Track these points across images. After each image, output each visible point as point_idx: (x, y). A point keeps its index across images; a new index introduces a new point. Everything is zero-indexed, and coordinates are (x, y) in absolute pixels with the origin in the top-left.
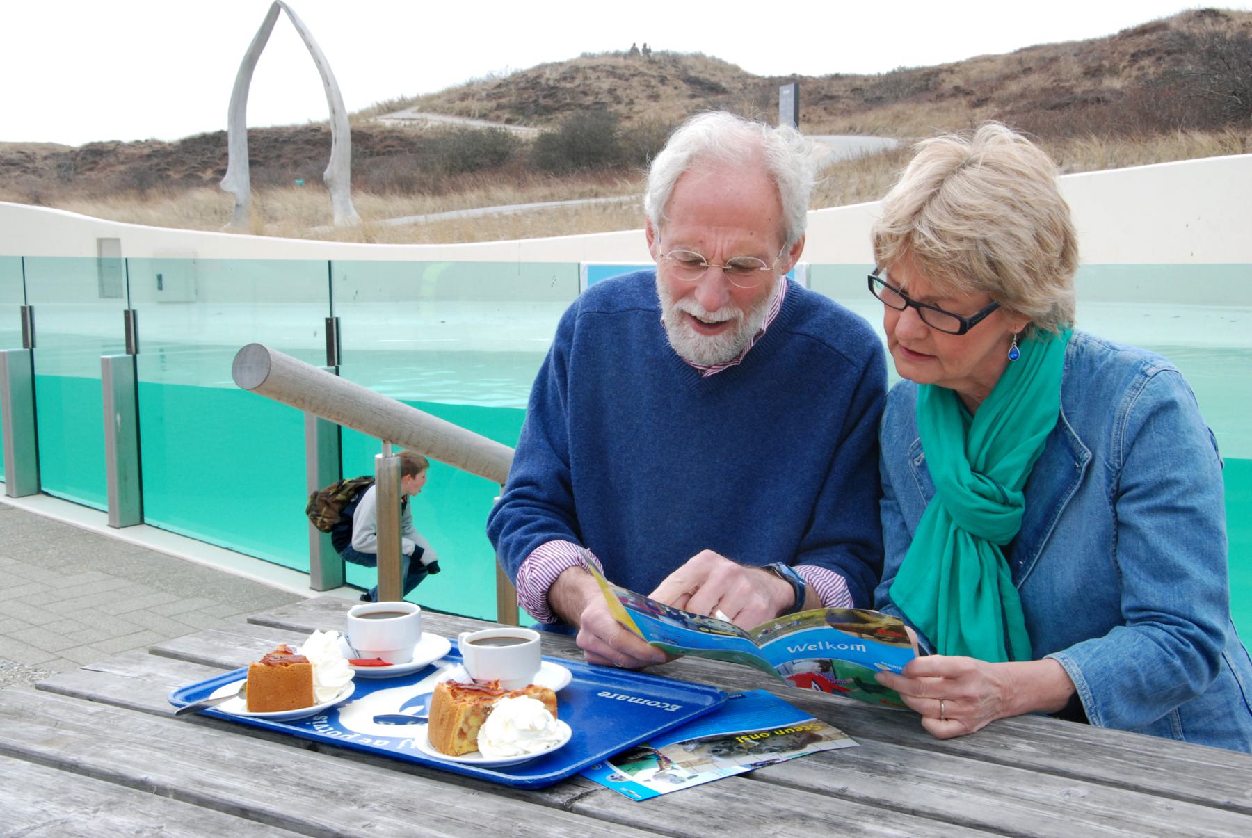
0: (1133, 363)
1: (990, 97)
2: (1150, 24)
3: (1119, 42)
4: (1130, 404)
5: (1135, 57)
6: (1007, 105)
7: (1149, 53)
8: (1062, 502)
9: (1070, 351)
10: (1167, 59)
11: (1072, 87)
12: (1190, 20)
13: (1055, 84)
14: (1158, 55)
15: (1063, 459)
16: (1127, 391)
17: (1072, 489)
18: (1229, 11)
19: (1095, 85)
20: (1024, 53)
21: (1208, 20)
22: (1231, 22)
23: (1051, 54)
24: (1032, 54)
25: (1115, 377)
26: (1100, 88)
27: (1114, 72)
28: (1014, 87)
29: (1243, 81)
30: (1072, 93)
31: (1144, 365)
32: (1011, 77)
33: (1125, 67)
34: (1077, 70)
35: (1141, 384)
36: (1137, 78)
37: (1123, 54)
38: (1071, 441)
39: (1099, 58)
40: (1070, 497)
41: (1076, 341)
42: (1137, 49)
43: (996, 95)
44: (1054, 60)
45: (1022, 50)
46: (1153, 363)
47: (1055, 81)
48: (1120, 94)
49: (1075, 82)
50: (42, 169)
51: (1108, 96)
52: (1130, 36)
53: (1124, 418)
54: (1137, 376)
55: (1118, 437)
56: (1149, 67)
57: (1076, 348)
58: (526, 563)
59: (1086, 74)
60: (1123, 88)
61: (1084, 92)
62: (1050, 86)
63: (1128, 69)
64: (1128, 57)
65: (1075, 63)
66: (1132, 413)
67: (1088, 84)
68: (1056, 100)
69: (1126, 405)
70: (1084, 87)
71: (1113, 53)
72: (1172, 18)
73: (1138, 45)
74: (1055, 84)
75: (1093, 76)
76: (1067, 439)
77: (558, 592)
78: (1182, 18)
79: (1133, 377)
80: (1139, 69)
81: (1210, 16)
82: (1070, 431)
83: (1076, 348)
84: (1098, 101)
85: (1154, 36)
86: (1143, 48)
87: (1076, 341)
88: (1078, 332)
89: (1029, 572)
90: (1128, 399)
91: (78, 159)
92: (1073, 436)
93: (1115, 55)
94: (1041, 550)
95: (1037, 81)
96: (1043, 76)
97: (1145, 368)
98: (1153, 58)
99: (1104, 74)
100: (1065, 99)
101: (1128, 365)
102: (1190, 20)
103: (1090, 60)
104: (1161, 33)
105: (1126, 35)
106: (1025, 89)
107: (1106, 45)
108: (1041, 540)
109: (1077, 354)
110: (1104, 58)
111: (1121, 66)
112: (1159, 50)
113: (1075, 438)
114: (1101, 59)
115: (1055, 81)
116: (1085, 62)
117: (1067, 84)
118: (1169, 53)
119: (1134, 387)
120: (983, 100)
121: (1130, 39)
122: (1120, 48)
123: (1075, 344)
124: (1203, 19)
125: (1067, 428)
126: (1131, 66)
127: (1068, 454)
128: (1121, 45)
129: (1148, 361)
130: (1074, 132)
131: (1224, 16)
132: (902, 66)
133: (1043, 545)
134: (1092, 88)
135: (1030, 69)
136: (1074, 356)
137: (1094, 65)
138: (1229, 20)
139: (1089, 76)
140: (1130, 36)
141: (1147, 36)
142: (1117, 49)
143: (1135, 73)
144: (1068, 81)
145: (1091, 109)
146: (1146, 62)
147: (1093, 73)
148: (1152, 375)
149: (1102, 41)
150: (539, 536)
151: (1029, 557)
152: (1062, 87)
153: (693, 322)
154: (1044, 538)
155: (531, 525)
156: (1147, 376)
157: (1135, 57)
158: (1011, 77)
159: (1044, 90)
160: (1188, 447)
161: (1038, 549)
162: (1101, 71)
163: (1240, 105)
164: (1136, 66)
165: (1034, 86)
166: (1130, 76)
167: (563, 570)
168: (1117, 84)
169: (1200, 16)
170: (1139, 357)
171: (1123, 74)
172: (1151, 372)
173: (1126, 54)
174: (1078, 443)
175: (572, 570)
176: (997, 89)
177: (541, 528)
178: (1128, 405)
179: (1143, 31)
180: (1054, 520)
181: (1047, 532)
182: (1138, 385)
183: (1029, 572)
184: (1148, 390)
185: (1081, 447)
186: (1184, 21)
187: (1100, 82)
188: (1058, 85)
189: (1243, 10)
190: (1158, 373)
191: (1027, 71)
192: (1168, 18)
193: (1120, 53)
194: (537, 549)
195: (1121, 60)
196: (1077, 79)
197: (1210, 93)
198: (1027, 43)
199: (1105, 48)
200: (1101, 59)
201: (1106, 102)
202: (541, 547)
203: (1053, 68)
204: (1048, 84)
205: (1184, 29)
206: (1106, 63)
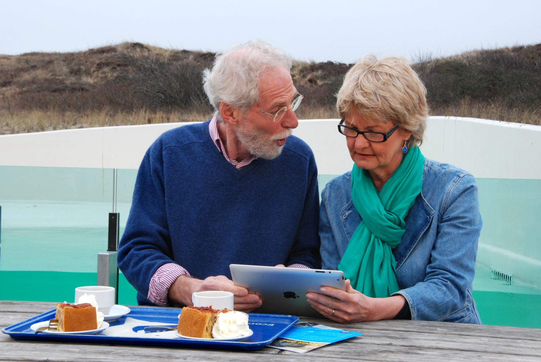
0: (454, 172)
1: (12, 81)
2: (106, 47)
3: (89, 56)
4: (452, 188)
5: (100, 66)
6: (24, 87)
7: (107, 64)
8: (420, 234)
9: (425, 169)
10: (118, 68)
11: (63, 80)
12: (128, 48)
13: (53, 77)
14: (112, 66)
15: (421, 214)
16: (451, 183)
17: (425, 228)
18: (149, 45)
19: (77, 80)
20: (29, 56)
21: (138, 50)
22: (150, 52)
23: (47, 59)
24: (34, 57)
25: (446, 179)
26: (80, 82)
27: (88, 73)
28: (27, 77)
29: (163, 85)
30: (64, 83)
31: (458, 173)
32: (23, 70)
33: (94, 71)
34: (65, 69)
35: (457, 180)
36: (102, 78)
37: (93, 63)
38: (425, 206)
39: (78, 64)
40: (424, 231)
41: (427, 164)
42: (100, 61)
43: (15, 80)
44: (51, 62)
45: (25, 55)
46: (462, 172)
47: (53, 75)
48: (93, 86)
49: (65, 77)
50: (169, 64)
51: (87, 87)
52: (95, 53)
53: (449, 193)
54: (455, 177)
55: (446, 201)
56: (108, 73)
57: (427, 167)
58: (155, 275)
59: (71, 72)
60: (94, 83)
61: (71, 83)
62: (50, 78)
63: (96, 73)
64: (95, 65)
65: (64, 66)
66: (453, 192)
67: (72, 79)
68: (55, 87)
69: (451, 188)
70: (71, 80)
71: (87, 62)
72: (118, 46)
73: (101, 59)
74: (53, 77)
75: (76, 74)
76: (424, 206)
77: (175, 288)
78: (124, 46)
79: (454, 177)
80: (102, 73)
81: (139, 47)
82: (425, 202)
83: (427, 167)
84: (82, 89)
85: (109, 55)
86: (103, 61)
87: (427, 164)
88: (427, 160)
89: (400, 267)
90: (452, 186)
91: (493, 63)
92: (427, 204)
93: (88, 63)
94: (407, 256)
95: (41, 74)
96: (45, 71)
97: (459, 174)
98: (110, 68)
99: (82, 74)
100: (60, 86)
101: (452, 173)
102: (128, 48)
103: (73, 64)
104: (113, 54)
105: (92, 52)
106: (34, 78)
107: (82, 57)
108: (408, 252)
109: (428, 170)
110: (81, 65)
111: (92, 70)
112: (113, 63)
113: (428, 205)
114: (80, 64)
115: (53, 75)
116: (70, 66)
117: (61, 78)
118: (119, 65)
119: (454, 181)
120: (7, 83)
121: (95, 55)
122: (91, 60)
123: (427, 166)
124: (136, 48)
125: (424, 201)
126: (98, 71)
127: (424, 212)
128: (91, 58)
129: (460, 171)
130: (69, 106)
131: (146, 48)
132: (330, 60)
133: (409, 254)
134: (76, 81)
135: (35, 66)
136: (427, 171)
137: (76, 68)
138: (149, 51)
139: (73, 74)
140: (95, 53)
141: (105, 54)
142: (88, 60)
143: (100, 75)
144: (61, 76)
145: (79, 94)
146: (106, 69)
147: (76, 72)
148: (462, 177)
149: (79, 54)
150: (159, 262)
151: (400, 260)
152: (58, 79)
153: (353, 142)
154: (410, 250)
155: (152, 256)
156: (460, 177)
157: (100, 66)
158: (23, 70)
159: (46, 80)
160: (472, 205)
161: (406, 256)
162: (80, 72)
163: (163, 99)
164: (101, 71)
165: (40, 77)
166: (98, 77)
167: (178, 277)
168: (90, 81)
169: (133, 47)
170: (456, 170)
171: (94, 75)
172: (461, 175)
173: (95, 63)
174: (429, 207)
175: (182, 277)
176: (16, 77)
177: (158, 258)
178: (452, 188)
179: (102, 51)
180: (415, 242)
181: (411, 248)
182: (456, 181)
183: (400, 267)
184: (461, 183)
185: (431, 208)
186: (125, 48)
187: (80, 79)
188: (55, 77)
189: (156, 46)
190: (464, 176)
191: (34, 67)
192: (115, 46)
193: (90, 62)
194: (161, 268)
195: (92, 67)
196: (66, 75)
197: (147, 91)
198: (29, 50)
199: (81, 59)
200: (80, 64)
201: (87, 90)
202: (162, 267)
203: (51, 67)
204: (49, 76)
205: (125, 52)
206: (83, 68)
